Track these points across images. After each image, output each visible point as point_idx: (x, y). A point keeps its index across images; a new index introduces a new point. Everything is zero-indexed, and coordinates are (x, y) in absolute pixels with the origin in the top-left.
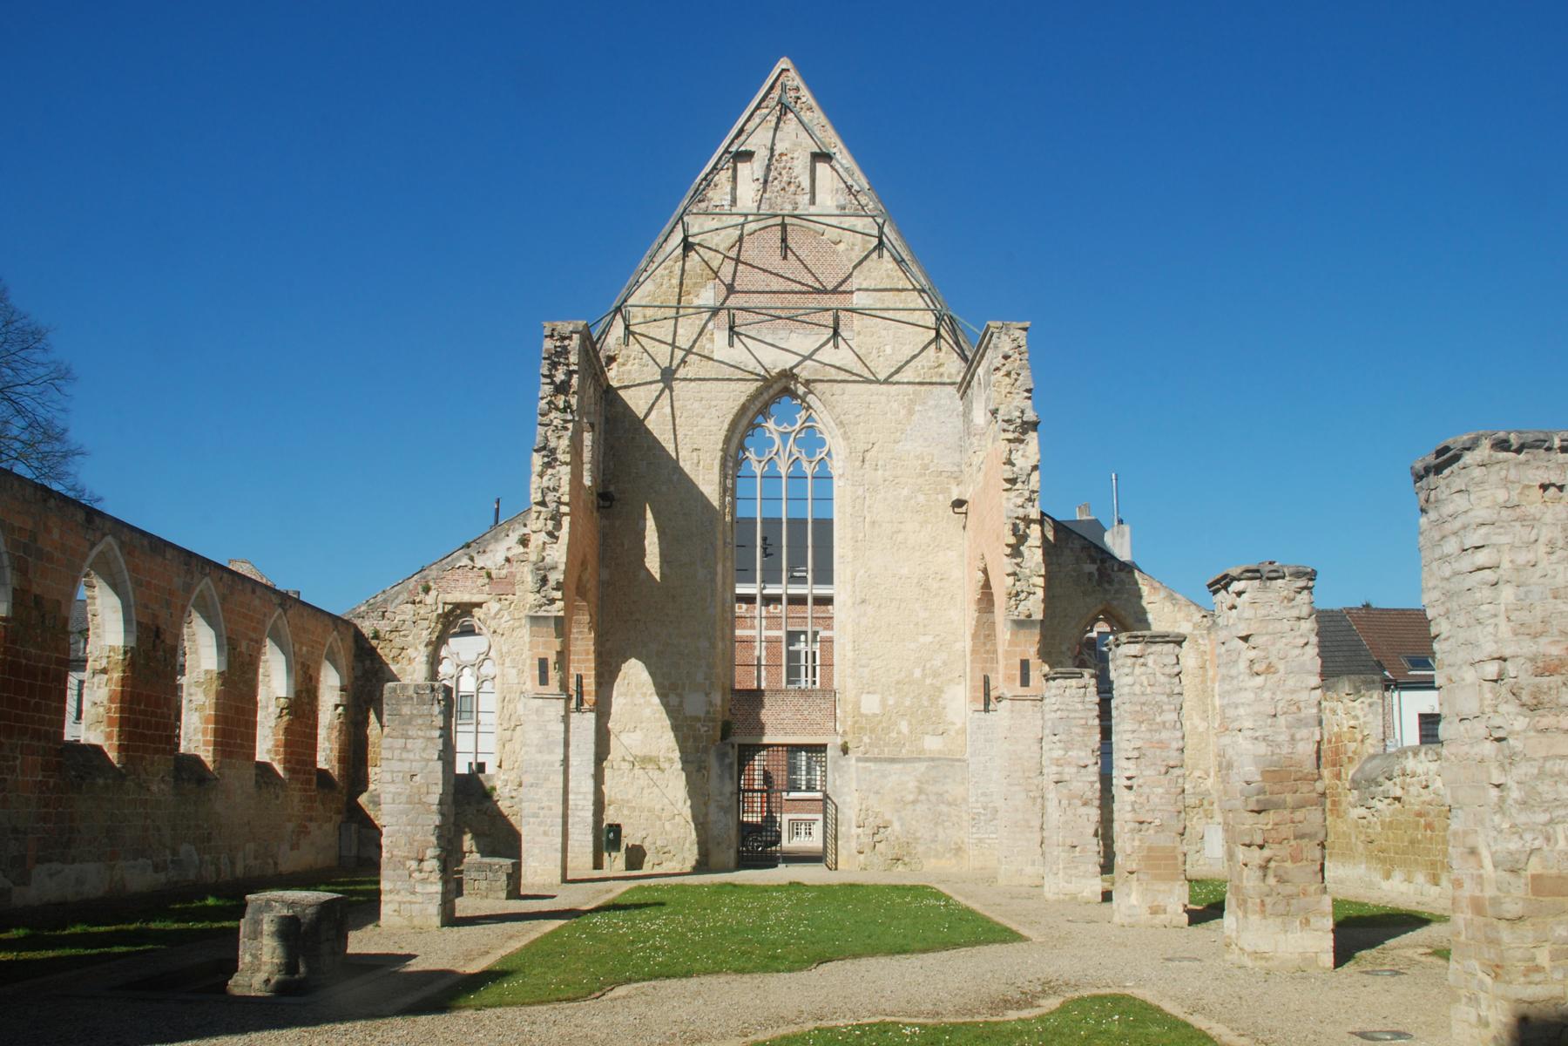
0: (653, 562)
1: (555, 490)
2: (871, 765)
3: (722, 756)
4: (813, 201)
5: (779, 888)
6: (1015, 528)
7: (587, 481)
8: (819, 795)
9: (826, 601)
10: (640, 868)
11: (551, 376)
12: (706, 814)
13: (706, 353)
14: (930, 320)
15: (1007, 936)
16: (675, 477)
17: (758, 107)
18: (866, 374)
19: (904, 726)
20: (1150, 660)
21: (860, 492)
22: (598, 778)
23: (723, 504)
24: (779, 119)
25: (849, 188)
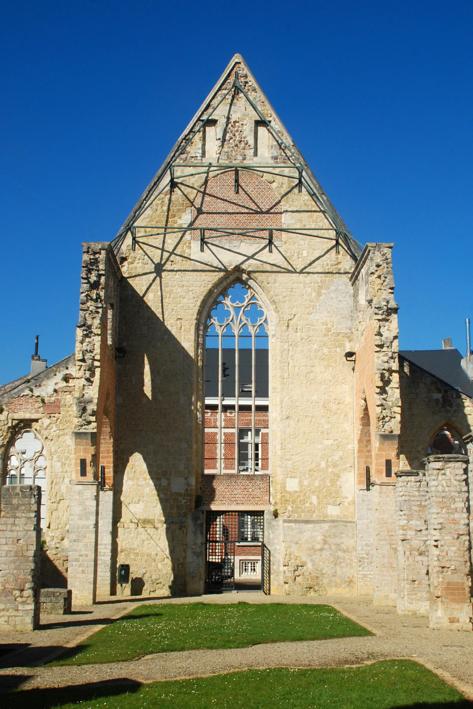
0: (148, 390)
1: (91, 352)
2: (293, 525)
3: (195, 519)
4: (256, 154)
5: (232, 606)
6: (382, 375)
7: (110, 342)
8: (260, 544)
9: (263, 409)
10: (140, 594)
11: (87, 278)
12: (185, 558)
13: (186, 255)
14: (332, 234)
15: (363, 632)
16: (166, 337)
17: (219, 89)
18: (290, 268)
19: (314, 499)
20: (448, 471)
21: (286, 346)
22: (114, 534)
23: (197, 355)
24: (233, 97)
25: (280, 145)
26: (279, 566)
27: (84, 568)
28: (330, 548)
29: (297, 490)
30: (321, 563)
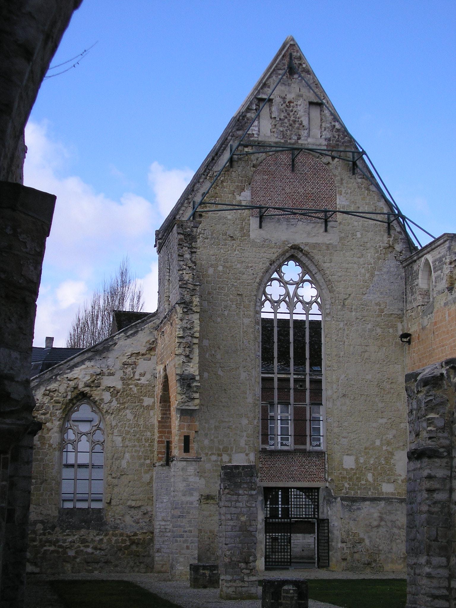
4: (309, 135)
26: (337, 542)
27: (188, 545)
28: (386, 525)
29: (354, 467)
30: (378, 540)
